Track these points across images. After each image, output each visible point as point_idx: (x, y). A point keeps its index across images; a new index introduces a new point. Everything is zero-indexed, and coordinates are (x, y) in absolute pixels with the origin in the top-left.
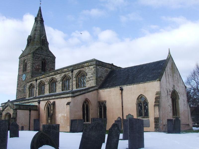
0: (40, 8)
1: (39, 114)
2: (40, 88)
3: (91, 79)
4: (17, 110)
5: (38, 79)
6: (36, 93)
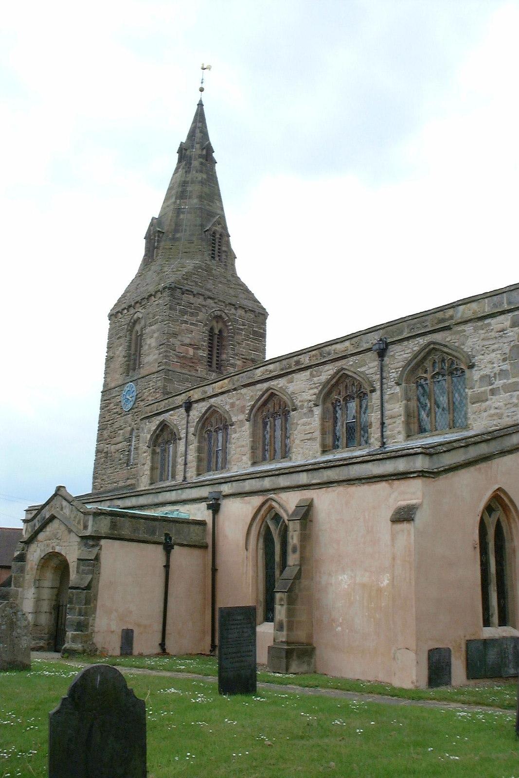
0: (200, 105)
1: (214, 570)
2: (205, 445)
3: (499, 383)
4: (103, 542)
5: (197, 401)
6: (186, 464)
